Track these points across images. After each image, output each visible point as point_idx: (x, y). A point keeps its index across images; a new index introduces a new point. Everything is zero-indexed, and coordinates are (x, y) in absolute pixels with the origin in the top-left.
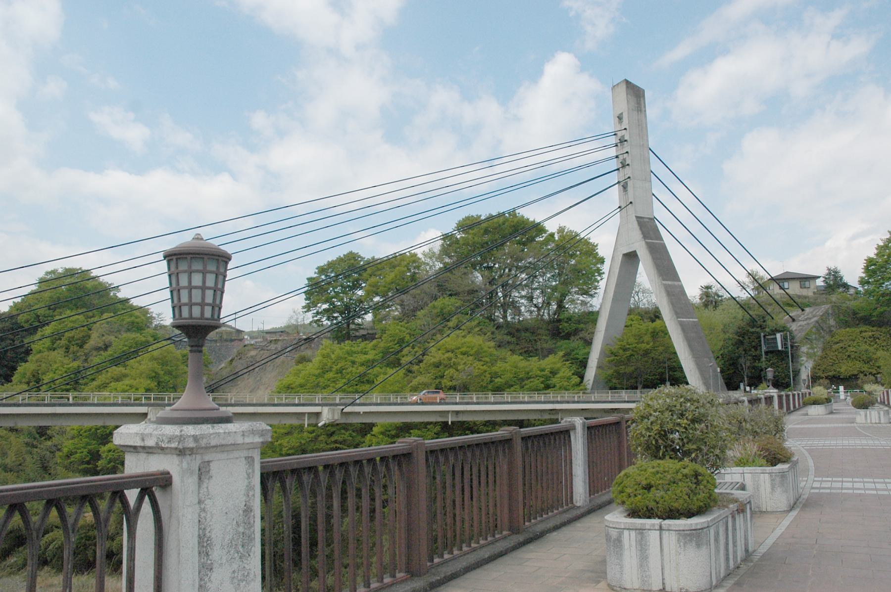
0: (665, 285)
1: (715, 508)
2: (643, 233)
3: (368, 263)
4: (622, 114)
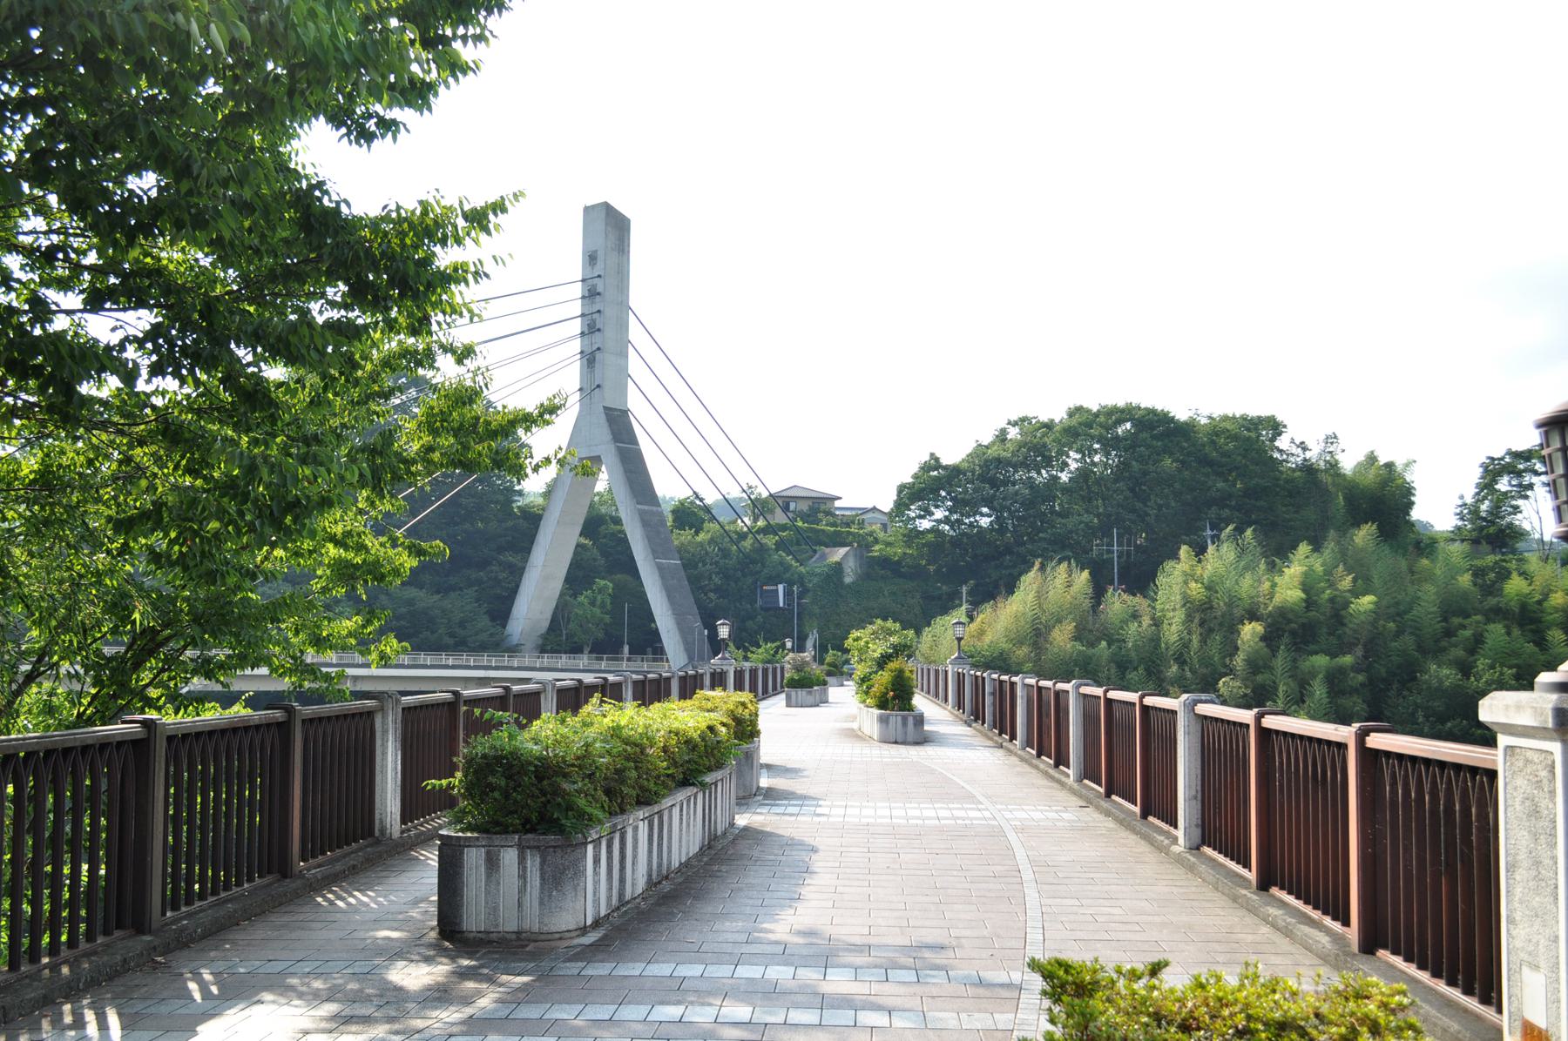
0: (639, 510)
1: (1362, 618)
2: (613, 433)
3: (895, 506)
4: (596, 251)
